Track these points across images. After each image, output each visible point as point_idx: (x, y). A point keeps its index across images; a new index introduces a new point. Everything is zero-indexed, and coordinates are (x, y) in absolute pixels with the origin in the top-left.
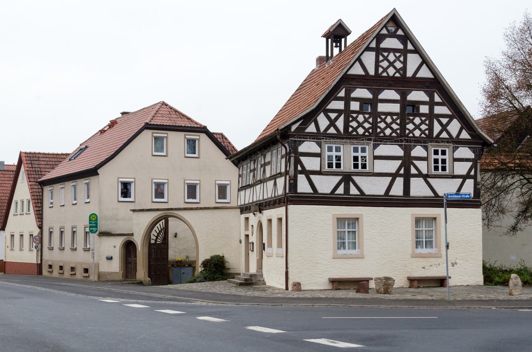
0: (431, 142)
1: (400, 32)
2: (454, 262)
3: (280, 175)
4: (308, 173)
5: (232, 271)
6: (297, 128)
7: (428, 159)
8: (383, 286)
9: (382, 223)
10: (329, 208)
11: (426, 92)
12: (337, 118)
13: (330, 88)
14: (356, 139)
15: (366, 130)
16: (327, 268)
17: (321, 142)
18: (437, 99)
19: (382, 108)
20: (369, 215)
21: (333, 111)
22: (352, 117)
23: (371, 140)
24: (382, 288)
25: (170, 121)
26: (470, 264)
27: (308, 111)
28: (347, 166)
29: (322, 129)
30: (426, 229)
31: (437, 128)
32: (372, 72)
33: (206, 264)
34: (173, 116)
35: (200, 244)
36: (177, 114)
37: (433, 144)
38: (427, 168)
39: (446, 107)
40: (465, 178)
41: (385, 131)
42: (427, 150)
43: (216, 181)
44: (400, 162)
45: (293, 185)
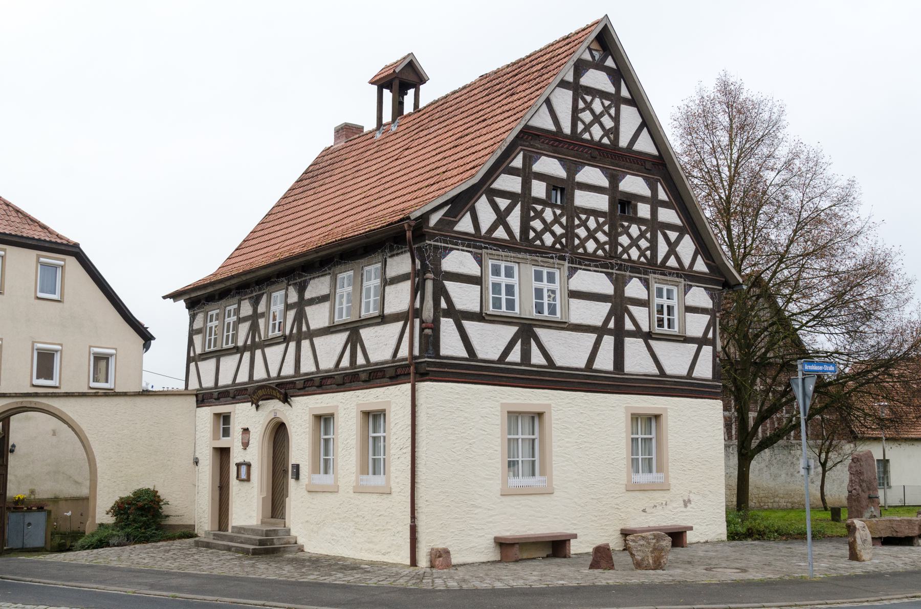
0: (655, 273)
1: (610, 62)
2: (686, 499)
3: (380, 320)
4: (459, 316)
5: (172, 521)
6: (440, 221)
7: (649, 304)
8: (652, 552)
9: (581, 422)
10: (495, 391)
11: (646, 179)
12: (509, 209)
13: (504, 145)
14: (541, 254)
15: (557, 239)
16: (491, 516)
17: (481, 254)
18: (662, 195)
19: (582, 199)
20: (561, 408)
21: (504, 194)
22: (535, 210)
23: (565, 260)
24: (650, 558)
25: (10, 228)
26: (708, 503)
27: (464, 187)
29: (484, 228)
30: (524, 437)
32: (567, 130)
33: (122, 509)
34: (13, 219)
35: (101, 467)
36: (21, 216)
37: (656, 276)
38: (648, 320)
39: (674, 211)
40: (701, 342)
41: (586, 244)
42: (648, 288)
43: (90, 347)
45: (431, 341)
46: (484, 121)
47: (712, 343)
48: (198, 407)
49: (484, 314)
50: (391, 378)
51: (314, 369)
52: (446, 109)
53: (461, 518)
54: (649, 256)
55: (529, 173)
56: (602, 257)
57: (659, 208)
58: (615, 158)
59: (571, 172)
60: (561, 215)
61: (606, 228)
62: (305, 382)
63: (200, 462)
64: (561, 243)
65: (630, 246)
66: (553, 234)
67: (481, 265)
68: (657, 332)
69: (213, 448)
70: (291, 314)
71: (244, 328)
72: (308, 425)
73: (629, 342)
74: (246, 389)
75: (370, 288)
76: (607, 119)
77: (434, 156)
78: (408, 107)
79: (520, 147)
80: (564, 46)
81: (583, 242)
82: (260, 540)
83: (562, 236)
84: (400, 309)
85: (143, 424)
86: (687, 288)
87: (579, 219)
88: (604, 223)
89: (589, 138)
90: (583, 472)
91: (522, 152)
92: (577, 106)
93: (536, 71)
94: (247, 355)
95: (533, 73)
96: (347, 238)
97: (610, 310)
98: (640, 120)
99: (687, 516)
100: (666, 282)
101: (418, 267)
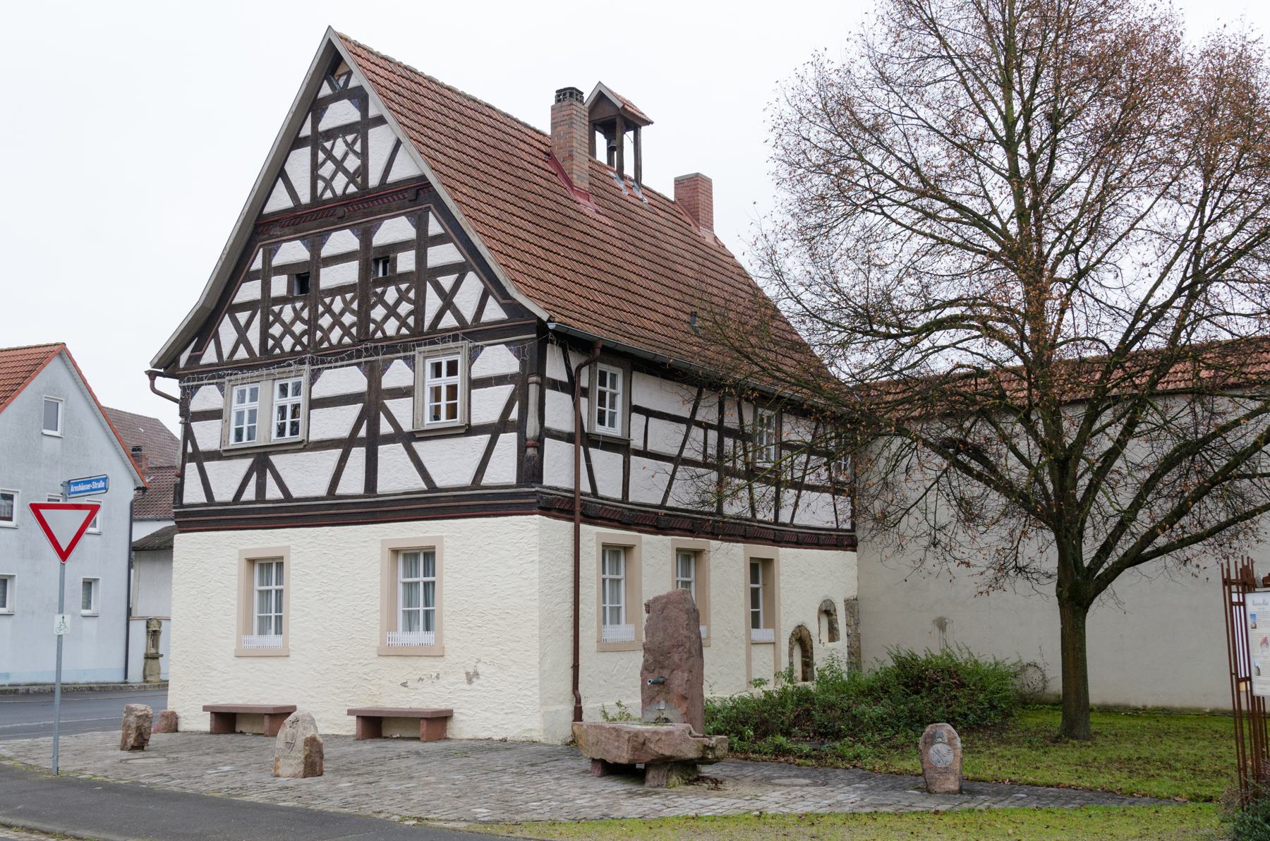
0: (419, 345)
2: (471, 671)
6: (190, 358)
20: (301, 549)
23: (304, 363)
28: (267, 434)
31: (433, 302)
37: (423, 348)
40: (494, 430)
44: (358, 407)
56: (349, 345)
97: (362, 412)
100: (445, 352)
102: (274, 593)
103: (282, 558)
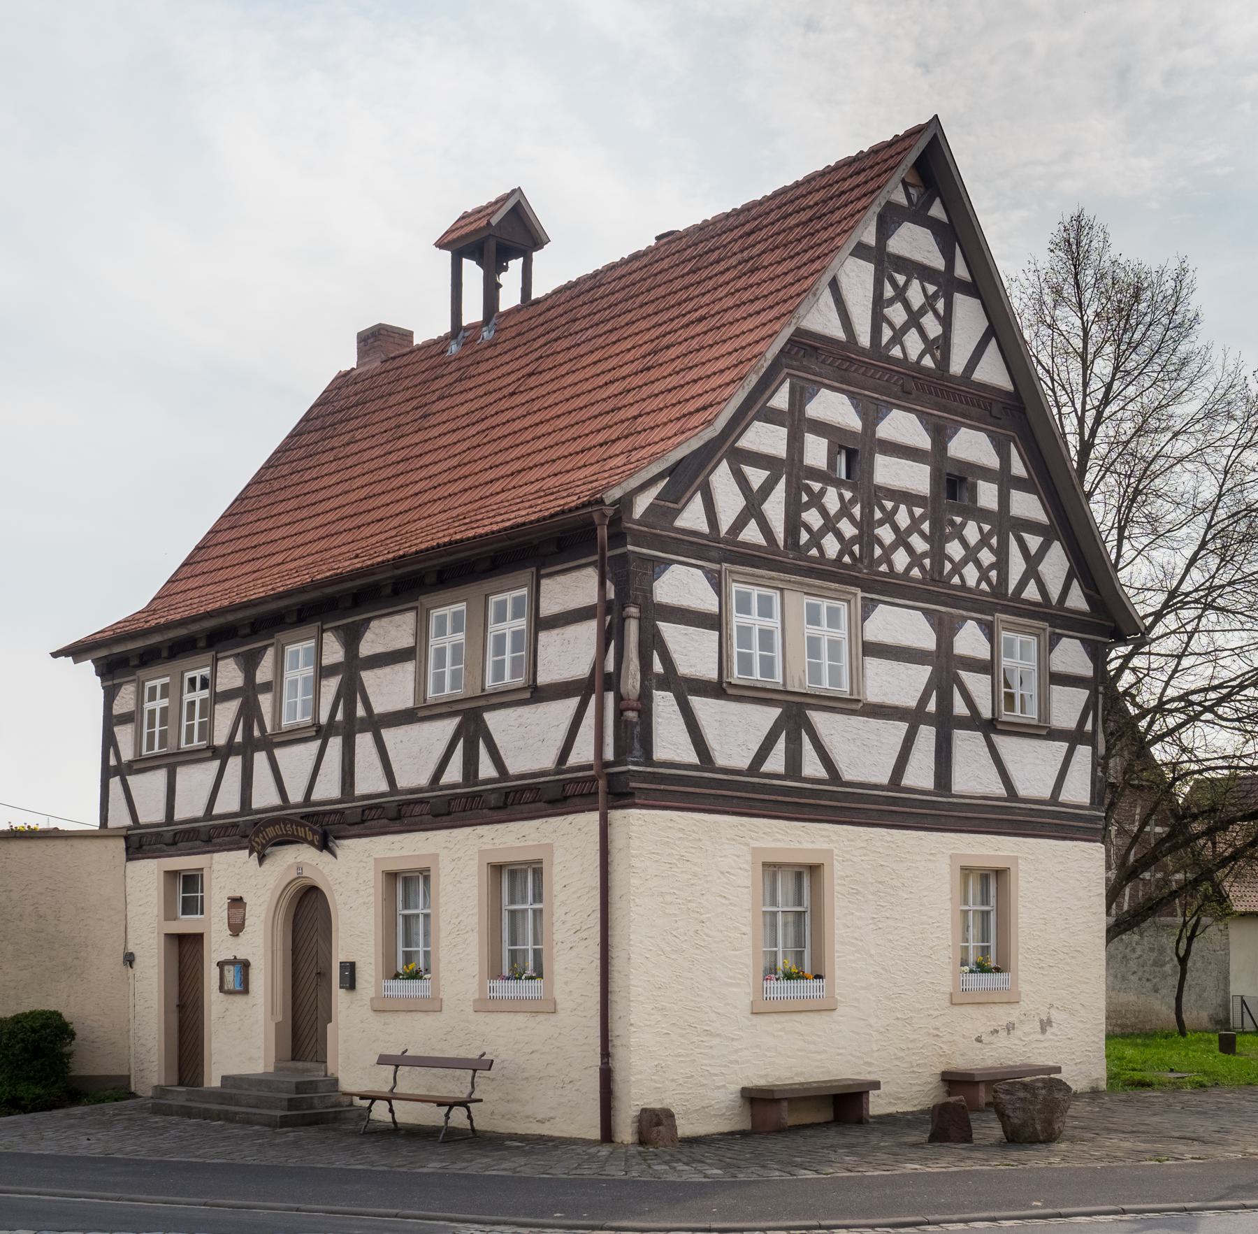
1: (937, 211)
7: (993, 668)
10: (742, 825)
11: (993, 437)
15: (846, 545)
16: (736, 1051)
17: (719, 572)
18: (1018, 468)
20: (848, 856)
22: (809, 490)
29: (725, 523)
32: (864, 340)
38: (990, 697)
39: (1036, 497)
40: (1074, 738)
46: (701, 319)
47: (1090, 740)
48: (129, 859)
49: (724, 685)
50: (551, 802)
51: (383, 787)
52: (602, 298)
53: (687, 1055)
54: (994, 580)
55: (799, 420)
57: (1013, 491)
58: (942, 394)
59: (871, 421)
60: (853, 501)
61: (926, 527)
62: (363, 811)
63: (138, 960)
64: (852, 554)
65: (964, 562)
66: (839, 535)
67: (719, 593)
68: (1004, 719)
69: (166, 935)
70: (331, 686)
71: (226, 715)
72: (372, 890)
73: (960, 737)
74: (235, 825)
75: (504, 635)
76: (931, 321)
77: (601, 387)
78: (509, 298)
79: (786, 370)
80: (851, 176)
81: (888, 551)
82: (290, 1100)
83: (854, 540)
84: (573, 673)
85: (25, 892)
86: (1054, 641)
87: (882, 508)
88: (923, 518)
89: (900, 355)
90: (882, 972)
91: (788, 380)
92: (882, 294)
93: (797, 225)
94: (235, 764)
95: (791, 229)
96: (462, 540)
98: (986, 324)
99: (1045, 1048)
101: (611, 595)
102: (530, 913)
103: (540, 862)
